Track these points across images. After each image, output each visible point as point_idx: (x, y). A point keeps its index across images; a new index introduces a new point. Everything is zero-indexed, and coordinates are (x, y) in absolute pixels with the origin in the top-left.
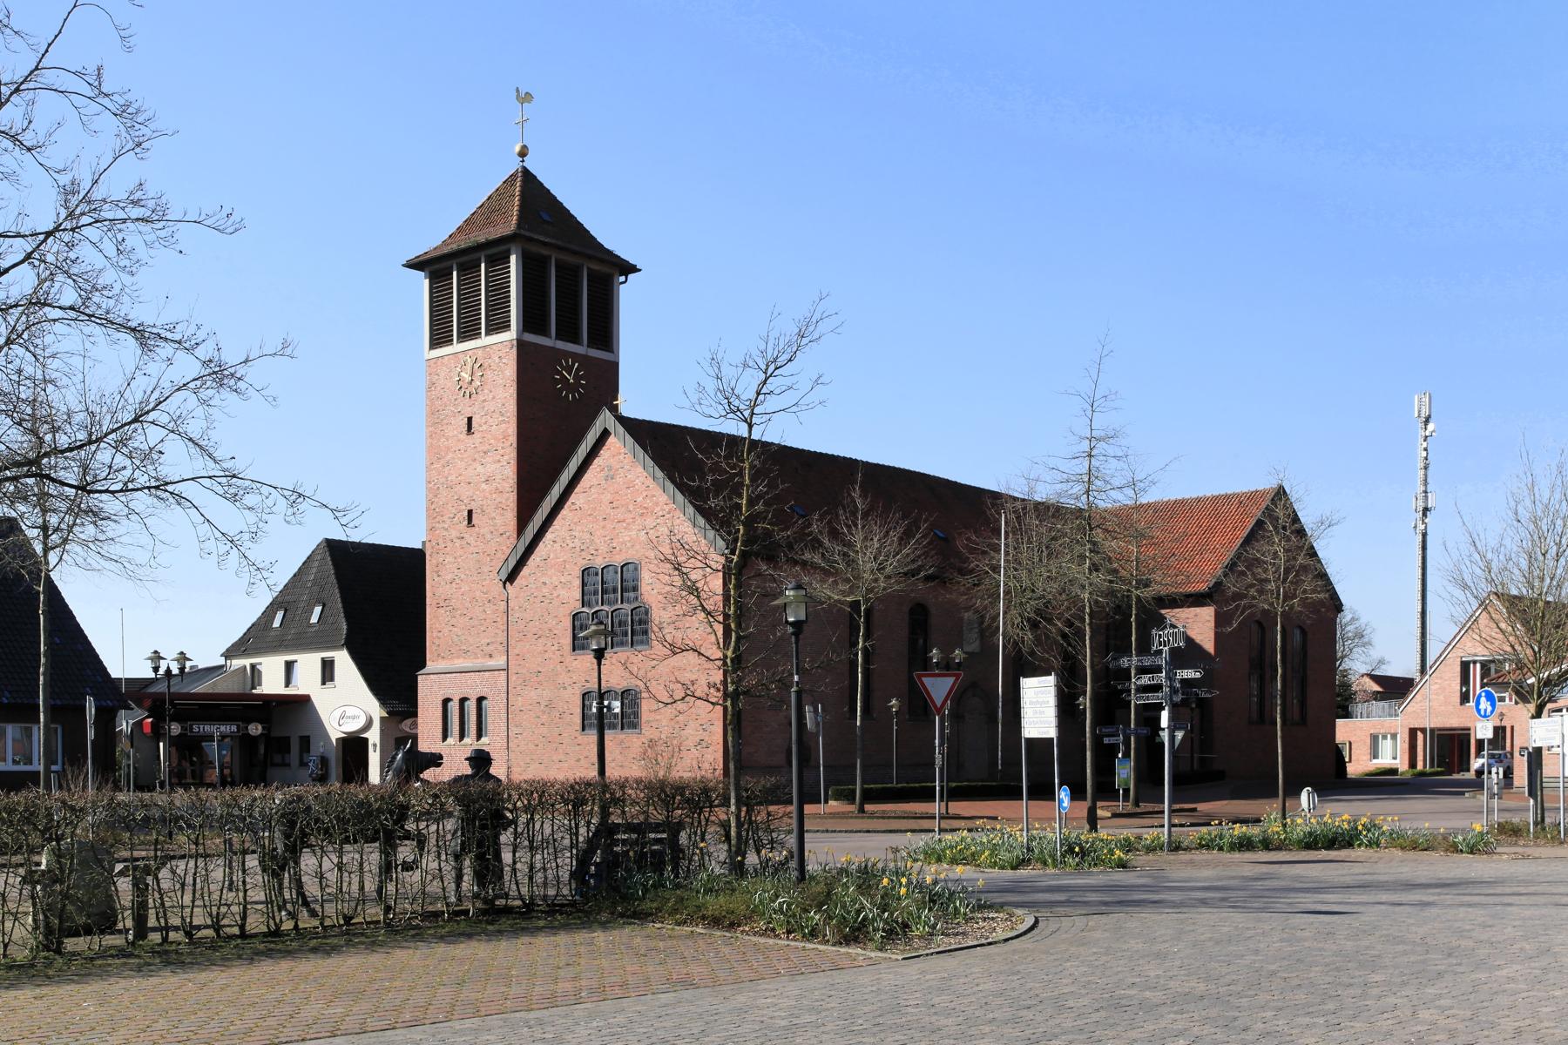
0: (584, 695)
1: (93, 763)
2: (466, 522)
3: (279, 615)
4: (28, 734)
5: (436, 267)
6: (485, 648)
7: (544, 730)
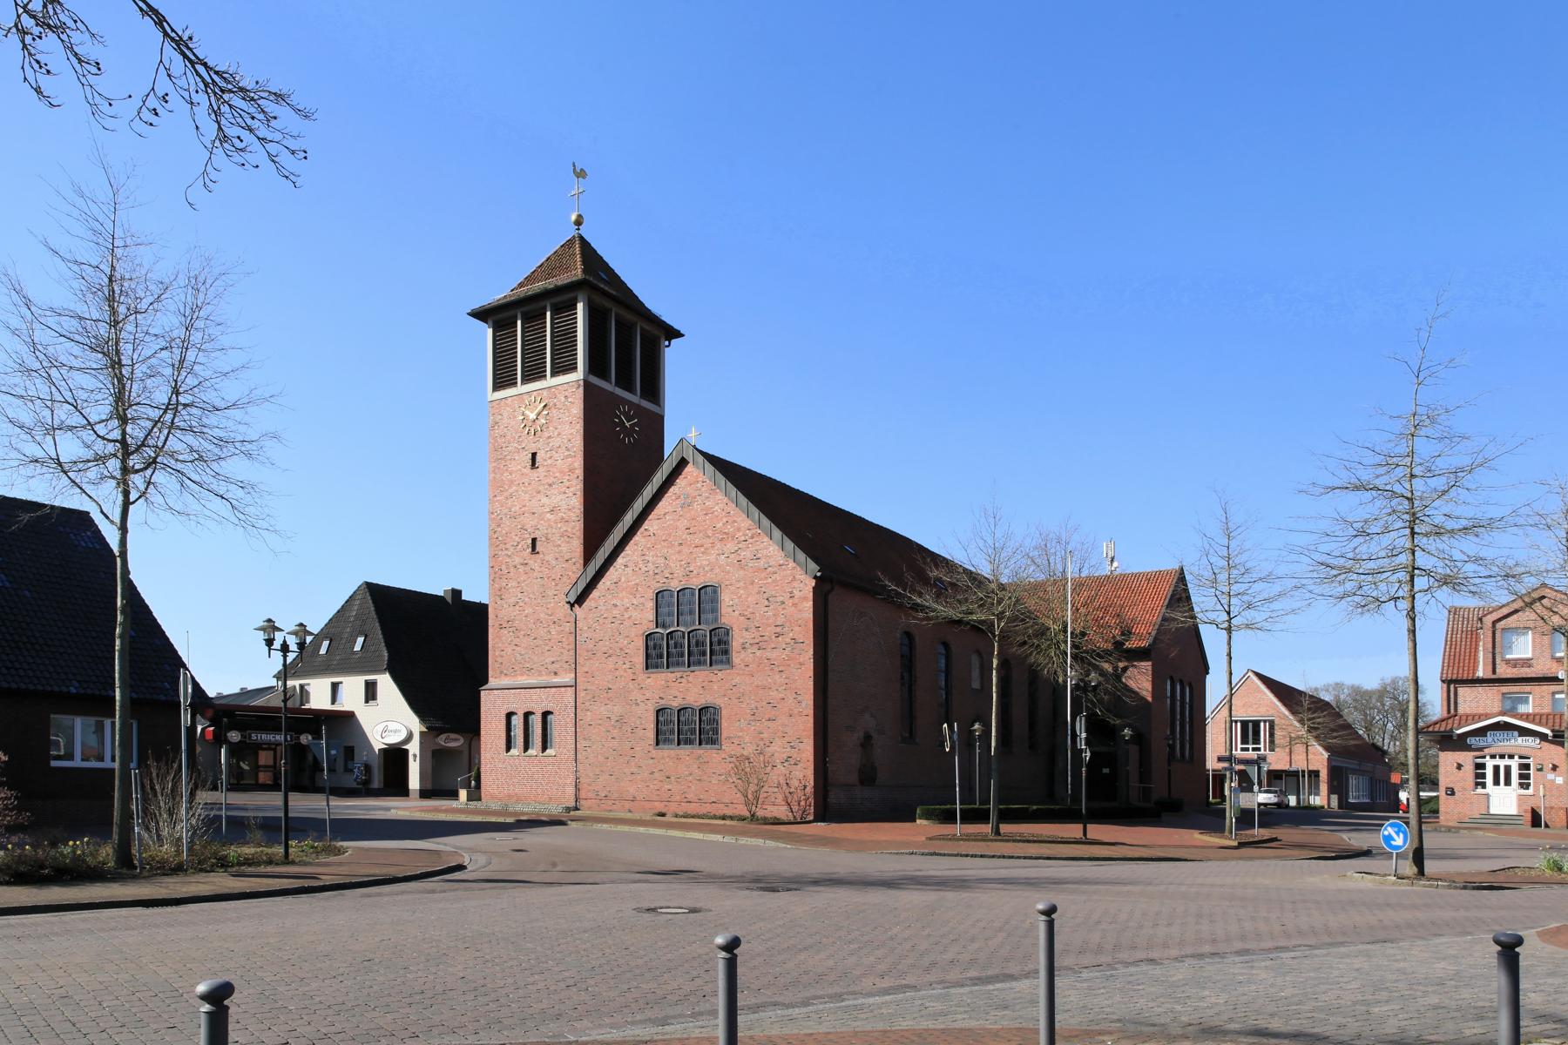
0: (658, 711)
2: (530, 549)
3: (326, 644)
4: (100, 729)
5: (500, 316)
7: (615, 743)
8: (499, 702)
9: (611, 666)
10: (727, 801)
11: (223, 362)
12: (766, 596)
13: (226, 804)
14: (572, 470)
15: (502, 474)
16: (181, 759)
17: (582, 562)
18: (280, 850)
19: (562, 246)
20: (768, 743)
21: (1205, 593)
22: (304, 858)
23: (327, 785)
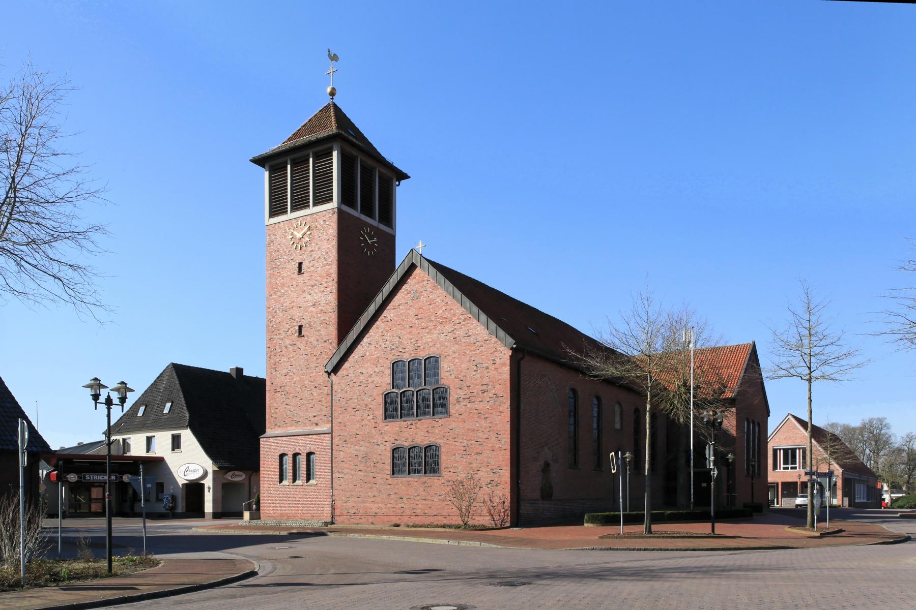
0: (394, 450)
1: (25, 494)
2: (297, 334)
3: (142, 408)
6: (312, 419)
7: (361, 474)
8: (274, 446)
9: (359, 418)
10: (445, 514)
11: (56, 165)
12: (475, 363)
13: (61, 528)
14: (329, 275)
15: (276, 279)
16: (20, 495)
17: (337, 342)
18: (104, 564)
19: (320, 111)
20: (476, 471)
21: (794, 354)
22: (125, 570)
23: (144, 512)
